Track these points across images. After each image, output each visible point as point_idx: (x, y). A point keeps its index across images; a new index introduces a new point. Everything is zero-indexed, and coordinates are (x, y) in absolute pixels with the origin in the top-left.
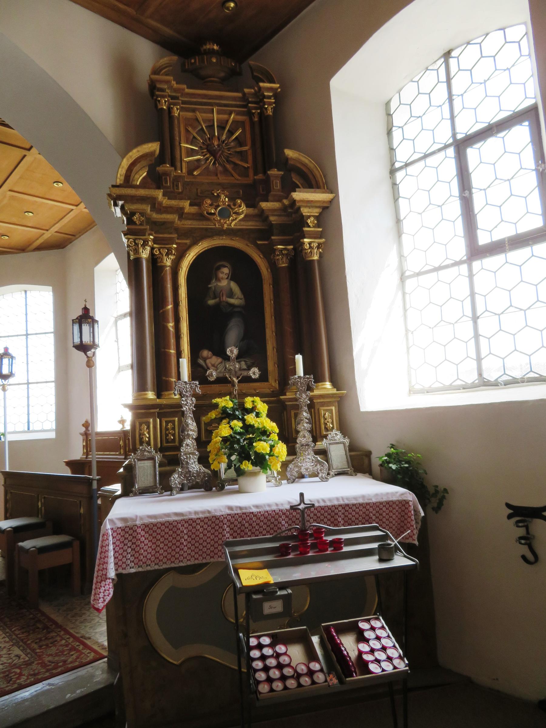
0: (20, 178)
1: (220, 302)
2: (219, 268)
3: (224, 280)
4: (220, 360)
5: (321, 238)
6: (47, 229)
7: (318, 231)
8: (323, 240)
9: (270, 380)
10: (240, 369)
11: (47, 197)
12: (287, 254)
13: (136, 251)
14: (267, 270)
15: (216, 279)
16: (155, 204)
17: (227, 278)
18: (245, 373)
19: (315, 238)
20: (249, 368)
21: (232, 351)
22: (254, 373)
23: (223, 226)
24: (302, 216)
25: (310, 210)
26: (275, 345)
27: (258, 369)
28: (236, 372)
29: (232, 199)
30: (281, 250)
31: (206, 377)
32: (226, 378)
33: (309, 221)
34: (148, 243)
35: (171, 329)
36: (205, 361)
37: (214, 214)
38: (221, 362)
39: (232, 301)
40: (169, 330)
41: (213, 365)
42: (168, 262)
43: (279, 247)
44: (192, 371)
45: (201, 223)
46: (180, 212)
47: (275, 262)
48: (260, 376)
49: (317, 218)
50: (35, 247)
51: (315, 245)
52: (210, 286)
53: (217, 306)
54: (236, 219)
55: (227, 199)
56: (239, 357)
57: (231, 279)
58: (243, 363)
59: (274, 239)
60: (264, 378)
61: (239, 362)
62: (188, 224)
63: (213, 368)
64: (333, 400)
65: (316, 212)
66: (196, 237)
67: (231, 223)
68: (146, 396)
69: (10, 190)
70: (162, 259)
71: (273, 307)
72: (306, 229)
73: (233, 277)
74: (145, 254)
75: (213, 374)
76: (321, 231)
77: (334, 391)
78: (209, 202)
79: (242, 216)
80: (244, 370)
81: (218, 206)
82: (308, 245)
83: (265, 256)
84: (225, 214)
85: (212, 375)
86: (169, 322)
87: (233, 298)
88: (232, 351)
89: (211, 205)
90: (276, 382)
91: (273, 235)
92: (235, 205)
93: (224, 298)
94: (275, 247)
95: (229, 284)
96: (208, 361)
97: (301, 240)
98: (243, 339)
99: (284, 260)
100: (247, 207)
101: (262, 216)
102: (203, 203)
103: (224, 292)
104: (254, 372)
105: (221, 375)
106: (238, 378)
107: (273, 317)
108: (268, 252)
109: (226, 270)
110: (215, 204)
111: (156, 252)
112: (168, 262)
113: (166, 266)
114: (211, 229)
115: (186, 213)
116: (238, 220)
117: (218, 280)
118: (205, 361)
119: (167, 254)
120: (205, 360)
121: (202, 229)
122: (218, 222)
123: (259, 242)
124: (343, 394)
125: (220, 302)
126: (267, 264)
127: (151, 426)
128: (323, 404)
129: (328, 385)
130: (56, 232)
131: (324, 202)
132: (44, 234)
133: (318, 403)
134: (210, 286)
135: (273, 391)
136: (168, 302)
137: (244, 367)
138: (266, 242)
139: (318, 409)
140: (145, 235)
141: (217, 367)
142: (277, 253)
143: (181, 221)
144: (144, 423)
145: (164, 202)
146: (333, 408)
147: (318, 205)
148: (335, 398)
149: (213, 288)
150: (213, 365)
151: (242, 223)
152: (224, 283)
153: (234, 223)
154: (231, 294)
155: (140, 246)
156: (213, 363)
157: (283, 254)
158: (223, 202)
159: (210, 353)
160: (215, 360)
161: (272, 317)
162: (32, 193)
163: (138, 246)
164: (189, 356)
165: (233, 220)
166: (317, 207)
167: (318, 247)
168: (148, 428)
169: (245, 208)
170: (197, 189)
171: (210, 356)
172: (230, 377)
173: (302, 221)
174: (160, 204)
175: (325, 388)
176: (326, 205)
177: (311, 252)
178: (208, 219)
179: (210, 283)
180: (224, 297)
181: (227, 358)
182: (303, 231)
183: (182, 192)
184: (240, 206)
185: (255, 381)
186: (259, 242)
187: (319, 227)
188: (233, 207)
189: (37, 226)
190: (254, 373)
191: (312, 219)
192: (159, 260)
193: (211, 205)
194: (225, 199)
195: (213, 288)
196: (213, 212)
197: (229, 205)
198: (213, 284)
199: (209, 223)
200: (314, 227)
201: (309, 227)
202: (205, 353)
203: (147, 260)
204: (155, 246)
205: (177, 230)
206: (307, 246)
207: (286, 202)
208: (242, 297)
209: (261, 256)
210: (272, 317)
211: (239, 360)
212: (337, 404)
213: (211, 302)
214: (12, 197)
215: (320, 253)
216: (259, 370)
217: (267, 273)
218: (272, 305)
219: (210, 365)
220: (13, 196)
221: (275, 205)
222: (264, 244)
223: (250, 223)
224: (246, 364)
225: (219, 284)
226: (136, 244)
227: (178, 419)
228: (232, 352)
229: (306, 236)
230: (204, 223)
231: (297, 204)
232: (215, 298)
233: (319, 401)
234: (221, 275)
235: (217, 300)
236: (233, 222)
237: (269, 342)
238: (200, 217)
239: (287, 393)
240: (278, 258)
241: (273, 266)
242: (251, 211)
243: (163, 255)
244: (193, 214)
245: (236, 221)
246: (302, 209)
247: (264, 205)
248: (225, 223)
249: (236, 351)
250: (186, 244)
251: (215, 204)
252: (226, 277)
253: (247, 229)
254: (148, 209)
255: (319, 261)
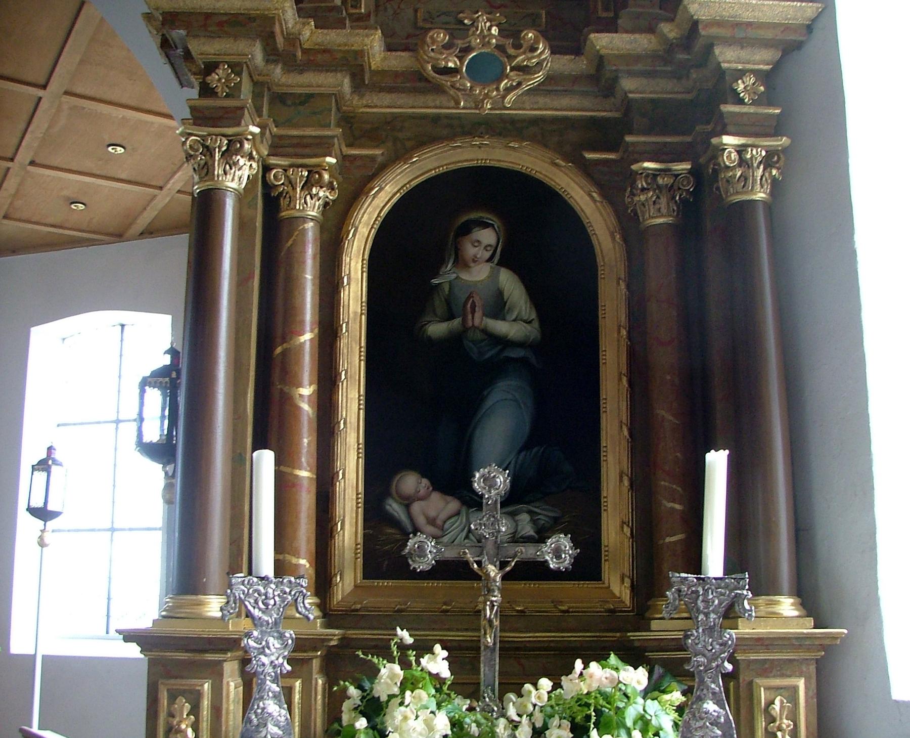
0: (82, 62)
1: (465, 329)
2: (466, 229)
3: (479, 266)
4: (453, 505)
5: (776, 132)
6: (160, 184)
7: (773, 115)
8: (784, 141)
9: (605, 575)
10: (516, 539)
11: (147, 106)
12: (671, 188)
13: (206, 170)
14: (613, 238)
15: (456, 262)
16: (272, 35)
17: (490, 260)
18: (527, 552)
19: (756, 135)
20: (541, 538)
21: (492, 481)
22: (557, 553)
23: (478, 105)
24: (720, 73)
25: (744, 54)
26: (626, 465)
27: (572, 540)
28: (498, 547)
29: (511, 33)
30: (655, 174)
31: (404, 559)
32: (467, 564)
33: (741, 87)
34: (242, 146)
35: (305, 406)
36: (407, 507)
37: (455, 71)
38: (458, 513)
39: (501, 327)
40: (299, 409)
41: (432, 522)
42: (310, 207)
43: (647, 165)
44: (365, 536)
45: (421, 99)
46: (353, 65)
47: (636, 214)
48: (577, 560)
49: (765, 77)
50: (141, 230)
51: (757, 154)
52: (435, 281)
53: (456, 340)
54: (519, 84)
55: (495, 31)
56: (512, 500)
57: (501, 264)
58: (525, 518)
59: (633, 144)
60: (587, 566)
61: (512, 515)
62: (381, 105)
63: (430, 529)
64: (802, 655)
65: (762, 59)
66: (401, 138)
67: (504, 97)
68: (197, 610)
69: (66, 93)
70: (292, 199)
71: (624, 349)
72: (729, 108)
73: (508, 257)
74: (236, 177)
75: (426, 551)
76: (778, 115)
77: (807, 628)
78: (442, 37)
79: (539, 77)
80: (527, 540)
81: (467, 50)
82: (734, 156)
83: (604, 195)
84: (486, 70)
85: (421, 550)
86: (300, 385)
87: (504, 319)
88: (492, 481)
89: (447, 46)
90: (623, 581)
91: (630, 133)
92: (517, 46)
93: (478, 319)
94: (634, 167)
95: (494, 276)
96: (416, 507)
97: (714, 141)
98: (527, 446)
99: (663, 201)
100: (553, 52)
101: (601, 79)
102: (424, 42)
103: (477, 299)
104: (559, 551)
105: (450, 554)
106: (503, 565)
107: (625, 379)
108: (613, 185)
109: (487, 237)
110: (460, 43)
111: (276, 177)
112: (310, 207)
113: (304, 219)
114: (448, 117)
115: (375, 73)
116: (525, 87)
117: (461, 263)
118: (407, 507)
119: (308, 185)
120: (407, 502)
121: (424, 117)
122: (470, 98)
123: (589, 156)
124: (834, 637)
125: (465, 329)
126: (613, 220)
127: (206, 703)
128: (767, 669)
129: (787, 606)
130: (179, 191)
131: (787, 28)
132: (155, 196)
133: (750, 662)
134: (435, 281)
135: (612, 611)
136: (302, 322)
137: (528, 530)
138: (612, 156)
139: (751, 683)
140: (239, 125)
141: (442, 528)
142: (641, 183)
143: (362, 96)
144: (183, 693)
145: (306, 33)
146: (801, 683)
147: (769, 34)
148: (809, 649)
149: (446, 288)
150: (432, 522)
151: (541, 100)
152: (479, 274)
153: (510, 98)
154: (499, 307)
155: (217, 156)
156: (432, 513)
157: (659, 187)
158: (483, 37)
159: (425, 482)
160: (439, 505)
161: (620, 379)
162: (114, 97)
163: (212, 156)
164: (361, 489)
165: (508, 90)
166: (767, 44)
167: (768, 163)
168: (195, 710)
169: (547, 53)
170: (416, 11)
171: (422, 492)
172: (479, 563)
173: (721, 87)
174: (292, 39)
175: (777, 615)
176: (792, 37)
177: (744, 177)
178: (439, 89)
179: (436, 275)
180: (478, 315)
181: (474, 502)
182: (721, 114)
183: (368, 15)
184: (533, 49)
185: (557, 575)
186: (589, 156)
187: (770, 104)
188: (511, 51)
189: (139, 179)
190: (557, 553)
191: (751, 80)
192: (283, 203)
193: (447, 46)
194: (490, 29)
195: (446, 288)
196: (451, 65)
197: (500, 48)
198: (447, 276)
199: (440, 100)
200: (754, 103)
201: (741, 102)
202: (411, 482)
203: (242, 198)
204: (273, 161)
205: (348, 120)
206: (730, 158)
207: (669, 30)
208: (534, 315)
209: (595, 195)
210: (620, 379)
211: (510, 509)
212: (813, 668)
213: (437, 329)
214: (73, 108)
215: (774, 181)
216: (576, 543)
217: (611, 245)
218: (624, 342)
219: (421, 521)
220: (75, 107)
221: (642, 42)
222: (606, 162)
223: (565, 101)
224: (534, 522)
225: (465, 276)
226: (209, 151)
227: (303, 683)
228: (489, 481)
229: (730, 128)
230: (430, 99)
231: (703, 33)
232: (450, 317)
233: (753, 657)
234: (470, 250)
235: (456, 323)
236: (509, 98)
237: (610, 458)
238: (418, 82)
239: (654, 625)
240: (643, 198)
241: (629, 225)
242: (566, 64)
243: (294, 189)
244: (396, 74)
245: (519, 91)
246: (717, 51)
247: (602, 41)
248: (487, 96)
249: (502, 480)
250: (372, 158)
251: (460, 43)
252: (488, 255)
253: (555, 120)
254: (257, 54)
255: (768, 206)
